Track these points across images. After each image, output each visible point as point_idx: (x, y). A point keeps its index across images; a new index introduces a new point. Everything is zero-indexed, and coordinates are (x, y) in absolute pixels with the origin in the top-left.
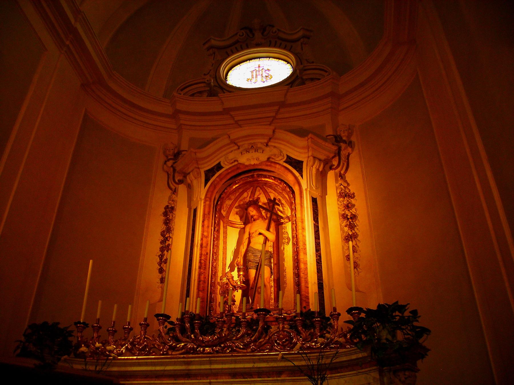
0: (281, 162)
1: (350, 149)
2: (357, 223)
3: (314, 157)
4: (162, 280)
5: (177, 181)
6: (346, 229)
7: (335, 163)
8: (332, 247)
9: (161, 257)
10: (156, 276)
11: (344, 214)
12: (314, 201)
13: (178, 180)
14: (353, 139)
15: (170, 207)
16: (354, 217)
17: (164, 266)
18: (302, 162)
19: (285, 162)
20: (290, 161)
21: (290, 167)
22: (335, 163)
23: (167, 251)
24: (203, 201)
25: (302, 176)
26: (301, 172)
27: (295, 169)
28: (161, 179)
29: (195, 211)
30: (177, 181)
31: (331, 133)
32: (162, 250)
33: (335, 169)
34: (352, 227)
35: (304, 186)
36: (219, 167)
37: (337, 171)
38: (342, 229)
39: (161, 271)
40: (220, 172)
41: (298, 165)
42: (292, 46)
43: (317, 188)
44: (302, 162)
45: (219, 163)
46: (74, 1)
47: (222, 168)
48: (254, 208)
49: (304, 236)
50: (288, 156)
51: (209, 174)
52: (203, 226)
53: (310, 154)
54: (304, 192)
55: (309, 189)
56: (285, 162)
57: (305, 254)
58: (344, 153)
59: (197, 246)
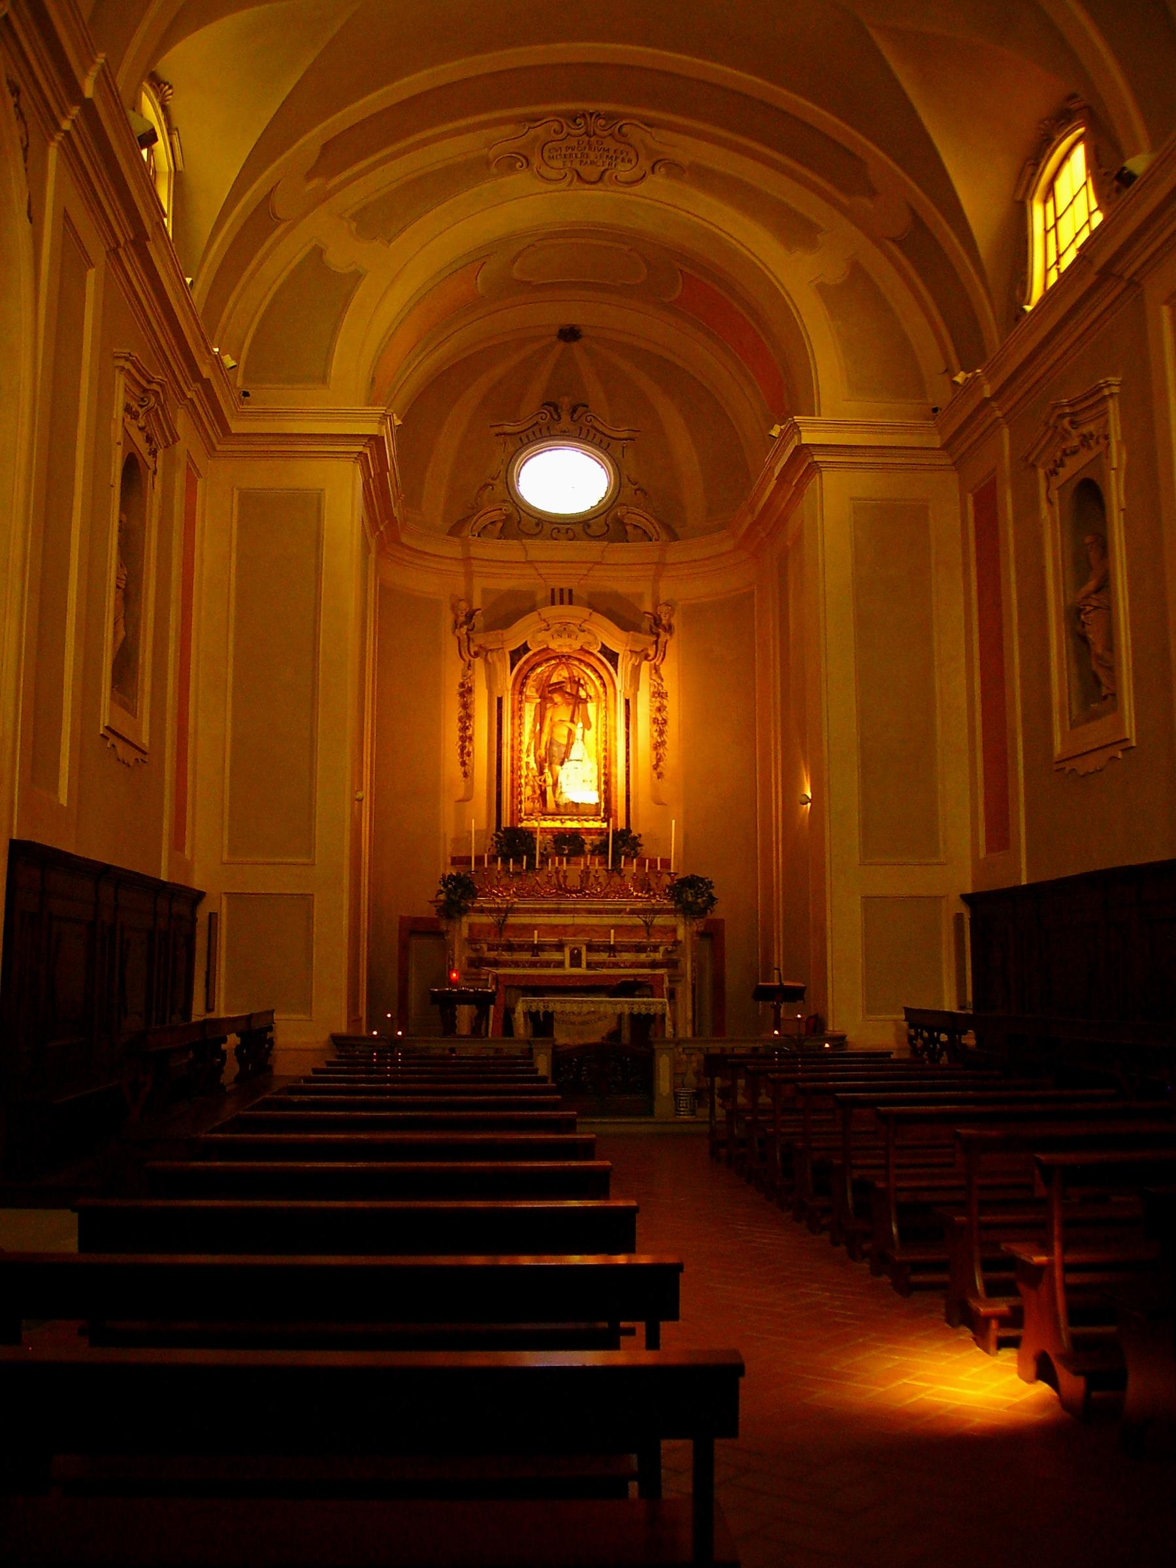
0: (595, 652)
1: (668, 637)
2: (666, 728)
3: (631, 651)
4: (465, 774)
5: (472, 654)
6: (656, 734)
7: (651, 653)
8: (639, 753)
9: (463, 748)
10: (459, 770)
11: (655, 718)
12: (627, 702)
13: (475, 652)
14: (674, 621)
15: (692, 891)
16: (665, 722)
17: (466, 758)
18: (618, 654)
19: (599, 651)
20: (605, 650)
21: (604, 660)
22: (651, 653)
23: (469, 742)
24: (510, 693)
25: (617, 673)
26: (615, 667)
27: (610, 662)
28: (450, 644)
29: (500, 700)
30: (472, 654)
31: (650, 610)
32: (463, 739)
33: (650, 661)
34: (661, 733)
35: (618, 687)
36: (525, 648)
37: (652, 662)
38: (652, 736)
39: (463, 764)
40: (527, 656)
41: (613, 657)
42: (609, 445)
43: (630, 686)
44: (618, 654)
45: (526, 643)
46: (72, 2)
47: (530, 650)
48: (560, 695)
49: (616, 746)
50: (603, 645)
51: (516, 655)
52: (513, 724)
53: (628, 648)
54: (618, 693)
55: (623, 691)
56: (599, 651)
57: (616, 766)
58: (662, 640)
59: (507, 747)
